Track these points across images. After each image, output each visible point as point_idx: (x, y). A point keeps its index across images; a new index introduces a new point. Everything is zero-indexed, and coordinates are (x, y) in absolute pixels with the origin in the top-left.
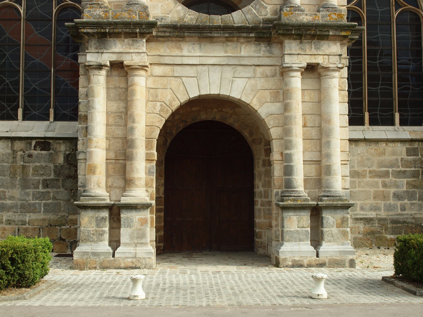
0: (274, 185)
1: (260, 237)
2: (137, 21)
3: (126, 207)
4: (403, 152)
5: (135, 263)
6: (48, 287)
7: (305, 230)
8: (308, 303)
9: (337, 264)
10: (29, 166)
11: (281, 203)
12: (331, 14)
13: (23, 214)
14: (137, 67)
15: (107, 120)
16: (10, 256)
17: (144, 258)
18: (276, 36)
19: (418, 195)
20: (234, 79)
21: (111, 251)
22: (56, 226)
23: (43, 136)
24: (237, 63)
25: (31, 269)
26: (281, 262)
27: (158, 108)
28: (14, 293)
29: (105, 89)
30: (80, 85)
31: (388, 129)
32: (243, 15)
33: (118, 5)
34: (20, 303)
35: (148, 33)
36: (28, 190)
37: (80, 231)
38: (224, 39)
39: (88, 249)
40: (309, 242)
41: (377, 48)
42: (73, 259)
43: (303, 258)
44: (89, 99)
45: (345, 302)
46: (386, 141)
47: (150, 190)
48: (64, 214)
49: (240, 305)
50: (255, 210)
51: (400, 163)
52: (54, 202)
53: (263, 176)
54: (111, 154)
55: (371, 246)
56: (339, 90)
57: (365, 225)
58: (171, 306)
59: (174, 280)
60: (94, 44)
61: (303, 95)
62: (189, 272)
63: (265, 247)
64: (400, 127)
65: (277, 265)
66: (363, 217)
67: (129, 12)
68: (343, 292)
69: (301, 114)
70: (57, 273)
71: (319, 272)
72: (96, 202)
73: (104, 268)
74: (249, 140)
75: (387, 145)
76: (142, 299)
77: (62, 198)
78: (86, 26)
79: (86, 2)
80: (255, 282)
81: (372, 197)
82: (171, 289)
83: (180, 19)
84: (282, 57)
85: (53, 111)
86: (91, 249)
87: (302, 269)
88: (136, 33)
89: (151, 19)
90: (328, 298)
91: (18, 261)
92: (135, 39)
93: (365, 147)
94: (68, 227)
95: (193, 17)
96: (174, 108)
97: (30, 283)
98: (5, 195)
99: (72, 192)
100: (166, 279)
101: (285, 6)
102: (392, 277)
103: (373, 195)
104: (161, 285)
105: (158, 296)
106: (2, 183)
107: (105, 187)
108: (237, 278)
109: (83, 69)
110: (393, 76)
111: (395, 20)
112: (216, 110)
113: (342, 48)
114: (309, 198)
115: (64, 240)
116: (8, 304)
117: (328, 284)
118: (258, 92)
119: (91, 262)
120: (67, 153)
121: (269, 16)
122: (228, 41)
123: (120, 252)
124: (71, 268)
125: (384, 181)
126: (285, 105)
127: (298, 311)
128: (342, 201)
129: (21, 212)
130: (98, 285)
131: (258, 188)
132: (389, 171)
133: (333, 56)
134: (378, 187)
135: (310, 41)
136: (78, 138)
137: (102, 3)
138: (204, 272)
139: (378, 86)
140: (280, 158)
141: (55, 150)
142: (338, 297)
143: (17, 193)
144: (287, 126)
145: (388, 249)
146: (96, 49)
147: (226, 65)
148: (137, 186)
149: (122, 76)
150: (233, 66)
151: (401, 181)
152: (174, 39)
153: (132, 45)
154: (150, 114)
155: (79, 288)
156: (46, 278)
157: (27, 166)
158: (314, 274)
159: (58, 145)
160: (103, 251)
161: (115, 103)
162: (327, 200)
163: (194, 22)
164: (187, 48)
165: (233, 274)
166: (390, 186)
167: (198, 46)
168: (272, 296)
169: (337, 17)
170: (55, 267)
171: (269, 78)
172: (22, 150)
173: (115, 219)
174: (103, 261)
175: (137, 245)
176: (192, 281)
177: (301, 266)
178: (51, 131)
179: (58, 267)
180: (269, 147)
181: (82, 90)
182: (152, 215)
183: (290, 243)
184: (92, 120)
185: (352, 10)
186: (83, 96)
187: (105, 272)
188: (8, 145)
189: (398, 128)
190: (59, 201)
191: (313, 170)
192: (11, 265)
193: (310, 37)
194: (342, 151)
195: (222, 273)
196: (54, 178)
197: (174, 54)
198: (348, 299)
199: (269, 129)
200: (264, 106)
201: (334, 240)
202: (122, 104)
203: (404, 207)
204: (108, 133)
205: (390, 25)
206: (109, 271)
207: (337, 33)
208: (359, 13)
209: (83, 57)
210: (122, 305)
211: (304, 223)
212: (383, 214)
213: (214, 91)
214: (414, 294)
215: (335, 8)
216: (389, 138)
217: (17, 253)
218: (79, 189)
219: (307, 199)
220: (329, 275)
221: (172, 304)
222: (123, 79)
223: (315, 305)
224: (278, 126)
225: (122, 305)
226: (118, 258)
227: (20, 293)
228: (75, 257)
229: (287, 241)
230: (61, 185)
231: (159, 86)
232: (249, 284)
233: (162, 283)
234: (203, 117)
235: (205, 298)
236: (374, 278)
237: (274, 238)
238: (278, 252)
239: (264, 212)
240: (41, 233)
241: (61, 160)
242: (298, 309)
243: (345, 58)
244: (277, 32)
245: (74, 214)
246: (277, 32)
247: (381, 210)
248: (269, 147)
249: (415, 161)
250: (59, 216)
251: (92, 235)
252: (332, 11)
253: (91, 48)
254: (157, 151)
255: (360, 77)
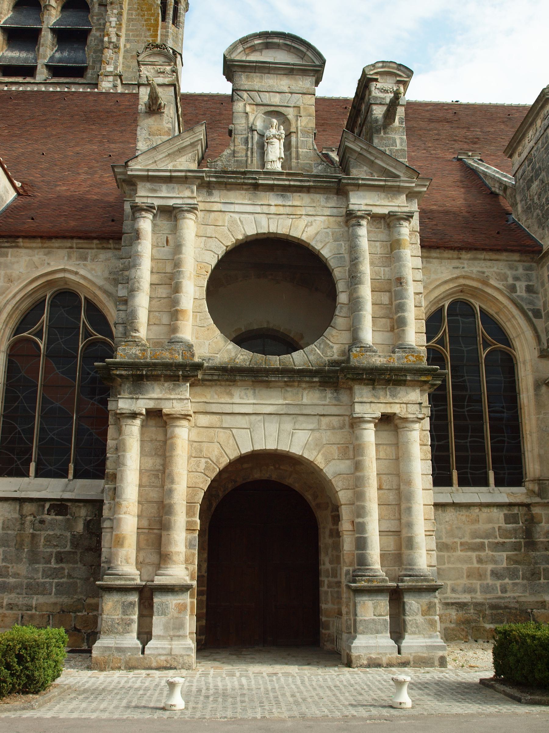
0: (344, 562)
1: (327, 628)
2: (180, 362)
3: (160, 589)
4: (500, 518)
5: (170, 661)
6: (61, 692)
7: (383, 619)
8: (388, 714)
9: (424, 662)
10: (40, 535)
11: (352, 585)
12: (408, 356)
13: (30, 596)
14: (178, 416)
15: (140, 480)
16: (17, 652)
17: (182, 656)
18: (344, 381)
19: (521, 573)
20: (294, 431)
21: (140, 646)
22: (70, 612)
23: (59, 497)
24: (299, 413)
25: (42, 670)
26: (354, 660)
27: (203, 466)
28: (19, 701)
29: (139, 442)
30: (109, 437)
31: (481, 491)
32: (305, 356)
33: (158, 343)
34: (27, 714)
35: (193, 376)
36: (37, 566)
37: (102, 620)
38: (283, 384)
39: (110, 643)
40: (389, 635)
41: (464, 393)
42: (90, 656)
43: (381, 656)
44: (119, 454)
45: (433, 712)
46: (480, 505)
47: (190, 567)
48: (81, 596)
49: (303, 717)
50: (321, 592)
51: (497, 533)
52: (68, 581)
53: (330, 551)
54: (143, 522)
55: (466, 638)
56: (420, 445)
57: (458, 611)
58: (217, 718)
59: (220, 684)
60: (128, 388)
61: (377, 451)
62: (238, 674)
63: (334, 640)
64: (496, 489)
65: (349, 664)
66: (455, 601)
67: (171, 350)
68: (431, 699)
69: (376, 473)
70: (71, 674)
71: (401, 673)
72: (123, 582)
73: (130, 668)
74: (313, 504)
75: (480, 510)
76: (181, 710)
77: (79, 577)
78: (119, 367)
79: (120, 339)
80: (321, 687)
81: (465, 576)
82: (216, 696)
83: (231, 359)
84: (351, 405)
85: (73, 466)
86: (115, 643)
87: (380, 669)
88: (179, 376)
89: (196, 360)
90: (413, 707)
91: (26, 658)
92: (177, 383)
93: (455, 513)
94: (85, 613)
95: (246, 357)
96: (222, 466)
97: (40, 687)
98: (8, 571)
99: (92, 569)
100: (209, 684)
101: (354, 346)
102: (491, 679)
103: (467, 573)
104: (203, 691)
105: (200, 706)
106: (6, 556)
107: (134, 563)
108: (299, 682)
109: (114, 418)
110: (485, 426)
111: (483, 361)
112: (272, 467)
113: (421, 395)
114: (387, 578)
115: (79, 631)
116: (12, 715)
117: (412, 689)
118: (323, 447)
119: (114, 660)
120: (89, 518)
121: (336, 357)
122: (288, 386)
123: (151, 648)
124: (89, 668)
125: (479, 555)
126: (356, 463)
127: (376, 724)
128: (428, 582)
129: (26, 594)
130: (124, 691)
131: (324, 564)
132: (484, 542)
133: (412, 405)
134: (472, 563)
135: (384, 387)
136: (103, 501)
137: (139, 340)
138: (257, 673)
139: (467, 439)
140: (351, 528)
141: (73, 514)
142: (425, 706)
143: (22, 568)
144: (358, 489)
145: (488, 642)
146: (130, 393)
147: (285, 414)
148: (175, 562)
149: (159, 427)
150: (294, 416)
151: (500, 556)
152: (223, 383)
153: (173, 389)
154: (192, 473)
155: (100, 694)
156: (58, 681)
157: (38, 535)
158: (395, 677)
159: (78, 509)
160: (130, 646)
161: (150, 458)
162: (410, 581)
163: (248, 363)
164: (238, 394)
165: (293, 676)
166: (486, 562)
167: (252, 392)
168: (343, 705)
169: (415, 360)
170: (68, 666)
171: (336, 431)
172: (32, 514)
173: (146, 604)
174: (130, 659)
175: (173, 638)
176: (243, 685)
177: (379, 665)
178: (70, 491)
179: (71, 667)
180: (337, 513)
181: (110, 443)
182: (192, 600)
183: (365, 636)
184: (122, 480)
185: (433, 349)
186: (112, 450)
187: (131, 674)
188: (15, 508)
189: (493, 490)
190: (75, 580)
191: (391, 541)
192: (17, 664)
193: (384, 382)
194: (426, 519)
195: (280, 675)
196: (71, 550)
197: (222, 400)
198: (437, 708)
199: (337, 492)
200: (330, 464)
201: (419, 632)
202: (159, 461)
203: (505, 588)
204: (140, 495)
205: (479, 366)
206: (136, 672)
207: (416, 378)
208: (441, 352)
209: (114, 403)
210: (156, 717)
211: (382, 609)
212: (479, 597)
213: (271, 446)
214: (519, 701)
215: (413, 348)
216: (482, 501)
217: (26, 649)
218: (102, 565)
219: (384, 579)
220: (414, 678)
221: (218, 715)
222: (161, 430)
223: (397, 717)
224: (348, 489)
225: (156, 717)
226: (148, 655)
227: (26, 701)
228: (95, 653)
229: (361, 634)
230: (79, 560)
231: (205, 440)
232: (315, 689)
233: (205, 688)
234: (257, 475)
235: (260, 708)
236: (470, 680)
237: (344, 629)
238: (350, 648)
239: (332, 596)
240: (51, 622)
241: (80, 527)
242: (376, 722)
243: (426, 407)
244: (345, 376)
245: (93, 597)
246: (345, 376)
247: (476, 592)
248: (337, 513)
249: (515, 530)
250: (75, 600)
251: (116, 625)
252: (409, 352)
253: (124, 393)
254: (200, 518)
255: (446, 428)
